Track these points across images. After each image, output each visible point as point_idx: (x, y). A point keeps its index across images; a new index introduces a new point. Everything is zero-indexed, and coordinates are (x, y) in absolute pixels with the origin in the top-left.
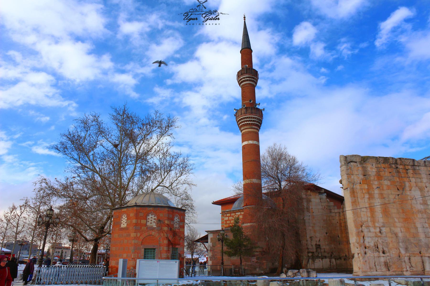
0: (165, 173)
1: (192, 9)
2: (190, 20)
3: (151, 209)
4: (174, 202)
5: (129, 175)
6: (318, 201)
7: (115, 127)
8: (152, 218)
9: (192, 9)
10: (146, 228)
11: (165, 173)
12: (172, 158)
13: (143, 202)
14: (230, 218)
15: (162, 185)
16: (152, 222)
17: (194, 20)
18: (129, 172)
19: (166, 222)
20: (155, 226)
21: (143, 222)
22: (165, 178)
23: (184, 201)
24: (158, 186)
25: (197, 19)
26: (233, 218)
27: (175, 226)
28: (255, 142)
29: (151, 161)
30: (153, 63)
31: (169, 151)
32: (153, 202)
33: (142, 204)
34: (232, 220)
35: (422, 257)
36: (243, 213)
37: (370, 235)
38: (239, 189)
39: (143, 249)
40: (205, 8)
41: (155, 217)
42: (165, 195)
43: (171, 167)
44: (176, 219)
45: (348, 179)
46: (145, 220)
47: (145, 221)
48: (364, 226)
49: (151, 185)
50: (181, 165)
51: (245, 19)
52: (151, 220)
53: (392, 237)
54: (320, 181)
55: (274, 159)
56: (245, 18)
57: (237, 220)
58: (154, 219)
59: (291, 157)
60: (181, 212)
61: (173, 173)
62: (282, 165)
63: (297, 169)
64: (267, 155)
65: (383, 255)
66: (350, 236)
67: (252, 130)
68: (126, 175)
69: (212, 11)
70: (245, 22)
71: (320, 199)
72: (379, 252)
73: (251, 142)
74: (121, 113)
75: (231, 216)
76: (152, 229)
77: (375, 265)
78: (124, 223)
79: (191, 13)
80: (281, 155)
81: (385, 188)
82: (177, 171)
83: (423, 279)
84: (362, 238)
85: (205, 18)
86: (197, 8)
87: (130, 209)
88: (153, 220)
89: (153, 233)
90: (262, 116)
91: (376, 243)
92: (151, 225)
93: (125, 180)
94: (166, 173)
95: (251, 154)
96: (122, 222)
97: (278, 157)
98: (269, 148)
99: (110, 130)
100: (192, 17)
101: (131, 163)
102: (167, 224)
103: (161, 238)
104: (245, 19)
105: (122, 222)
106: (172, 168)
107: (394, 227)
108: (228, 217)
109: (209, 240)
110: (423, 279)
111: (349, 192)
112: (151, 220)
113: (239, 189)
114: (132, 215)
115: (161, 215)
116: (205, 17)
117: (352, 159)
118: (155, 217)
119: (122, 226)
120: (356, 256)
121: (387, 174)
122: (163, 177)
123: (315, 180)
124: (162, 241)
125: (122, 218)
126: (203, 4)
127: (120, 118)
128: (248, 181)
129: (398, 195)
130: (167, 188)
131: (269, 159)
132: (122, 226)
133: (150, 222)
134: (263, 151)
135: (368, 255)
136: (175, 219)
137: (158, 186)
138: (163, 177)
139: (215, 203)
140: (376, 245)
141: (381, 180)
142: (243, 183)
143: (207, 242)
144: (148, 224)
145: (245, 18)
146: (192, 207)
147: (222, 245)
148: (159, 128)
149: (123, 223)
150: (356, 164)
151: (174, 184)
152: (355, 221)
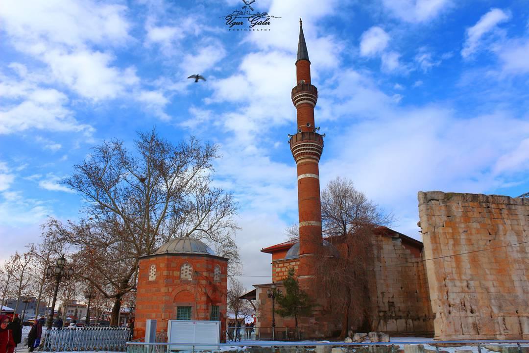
0: (202, 213)
1: (236, 11)
3: (186, 257)
4: (214, 249)
5: (158, 217)
6: (391, 248)
7: (141, 157)
8: (186, 269)
9: (236, 11)
10: (179, 281)
11: (202, 213)
12: (211, 195)
13: (176, 249)
14: (284, 269)
15: (199, 228)
16: (187, 274)
17: (239, 24)
18: (158, 212)
19: (205, 274)
20: (191, 279)
21: (176, 273)
22: (203, 219)
23: (227, 248)
24: (195, 229)
25: (242, 23)
26: (287, 270)
27: (215, 279)
28: (314, 176)
29: (185, 199)
30: (189, 78)
31: (208, 186)
32: (188, 249)
33: (175, 252)
34: (286, 271)
35: (519, 317)
36: (299, 263)
37: (455, 289)
38: (294, 234)
39: (176, 308)
40: (253, 10)
41: (191, 269)
42: (204, 241)
43: (210, 207)
44: (217, 270)
45: (428, 221)
46: (178, 271)
47: (179, 273)
48: (447, 278)
49: (186, 228)
50: (223, 204)
51: (301, 24)
52: (186, 272)
53: (482, 293)
54: (393, 223)
55: (337, 196)
56: (301, 22)
57: (291, 272)
58: (190, 270)
59: (358, 194)
60: (223, 262)
61: (212, 214)
62: (347, 204)
63: (366, 209)
64: (328, 191)
65: (472, 315)
66: (431, 291)
67: (310, 160)
68: (155, 216)
69: (261, 14)
70: (301, 27)
71: (394, 246)
72: (466, 311)
73: (308, 175)
74: (149, 140)
75: (284, 267)
76: (187, 282)
77: (461, 328)
78: (153, 275)
79: (235, 16)
80: (346, 191)
81: (474, 231)
82: (218, 211)
83: (520, 344)
84: (445, 293)
85: (253, 22)
86: (242, 10)
87: (160, 258)
88: (189, 272)
89: (189, 288)
90: (322, 143)
91: (462, 300)
92: (186, 277)
93: (154, 222)
94: (204, 214)
95: (309, 190)
96: (150, 274)
97: (342, 194)
98: (331, 182)
99: (135, 160)
100: (236, 21)
101: (161, 201)
102: (206, 277)
103: (198, 294)
104: (301, 24)
105: (150, 274)
106: (212, 207)
107: (485, 280)
108: (281, 267)
109: (257, 296)
110: (520, 344)
111: (429, 236)
112: (186, 272)
113: (294, 234)
114: (162, 265)
115: (198, 265)
116: (252, 21)
117: (433, 196)
118: (191, 269)
119: (150, 279)
120: (438, 315)
121: (476, 215)
122: (201, 219)
123: (388, 222)
124: (199, 297)
125: (150, 269)
126: (250, 5)
127: (148, 146)
128: (304, 224)
129: (490, 241)
130: (206, 232)
131: (331, 197)
132: (150, 279)
133: (185, 274)
134: (324, 187)
135: (453, 314)
136: (215, 270)
137: (195, 229)
138: (201, 219)
139: (253, 285)
140: (463, 302)
141: (469, 222)
142: (299, 225)
143: (255, 299)
144: (183, 276)
145: (301, 22)
146: (236, 255)
147: (274, 302)
148: (195, 158)
149: (152, 275)
150: (438, 202)
151: (215, 228)
152: (437, 273)
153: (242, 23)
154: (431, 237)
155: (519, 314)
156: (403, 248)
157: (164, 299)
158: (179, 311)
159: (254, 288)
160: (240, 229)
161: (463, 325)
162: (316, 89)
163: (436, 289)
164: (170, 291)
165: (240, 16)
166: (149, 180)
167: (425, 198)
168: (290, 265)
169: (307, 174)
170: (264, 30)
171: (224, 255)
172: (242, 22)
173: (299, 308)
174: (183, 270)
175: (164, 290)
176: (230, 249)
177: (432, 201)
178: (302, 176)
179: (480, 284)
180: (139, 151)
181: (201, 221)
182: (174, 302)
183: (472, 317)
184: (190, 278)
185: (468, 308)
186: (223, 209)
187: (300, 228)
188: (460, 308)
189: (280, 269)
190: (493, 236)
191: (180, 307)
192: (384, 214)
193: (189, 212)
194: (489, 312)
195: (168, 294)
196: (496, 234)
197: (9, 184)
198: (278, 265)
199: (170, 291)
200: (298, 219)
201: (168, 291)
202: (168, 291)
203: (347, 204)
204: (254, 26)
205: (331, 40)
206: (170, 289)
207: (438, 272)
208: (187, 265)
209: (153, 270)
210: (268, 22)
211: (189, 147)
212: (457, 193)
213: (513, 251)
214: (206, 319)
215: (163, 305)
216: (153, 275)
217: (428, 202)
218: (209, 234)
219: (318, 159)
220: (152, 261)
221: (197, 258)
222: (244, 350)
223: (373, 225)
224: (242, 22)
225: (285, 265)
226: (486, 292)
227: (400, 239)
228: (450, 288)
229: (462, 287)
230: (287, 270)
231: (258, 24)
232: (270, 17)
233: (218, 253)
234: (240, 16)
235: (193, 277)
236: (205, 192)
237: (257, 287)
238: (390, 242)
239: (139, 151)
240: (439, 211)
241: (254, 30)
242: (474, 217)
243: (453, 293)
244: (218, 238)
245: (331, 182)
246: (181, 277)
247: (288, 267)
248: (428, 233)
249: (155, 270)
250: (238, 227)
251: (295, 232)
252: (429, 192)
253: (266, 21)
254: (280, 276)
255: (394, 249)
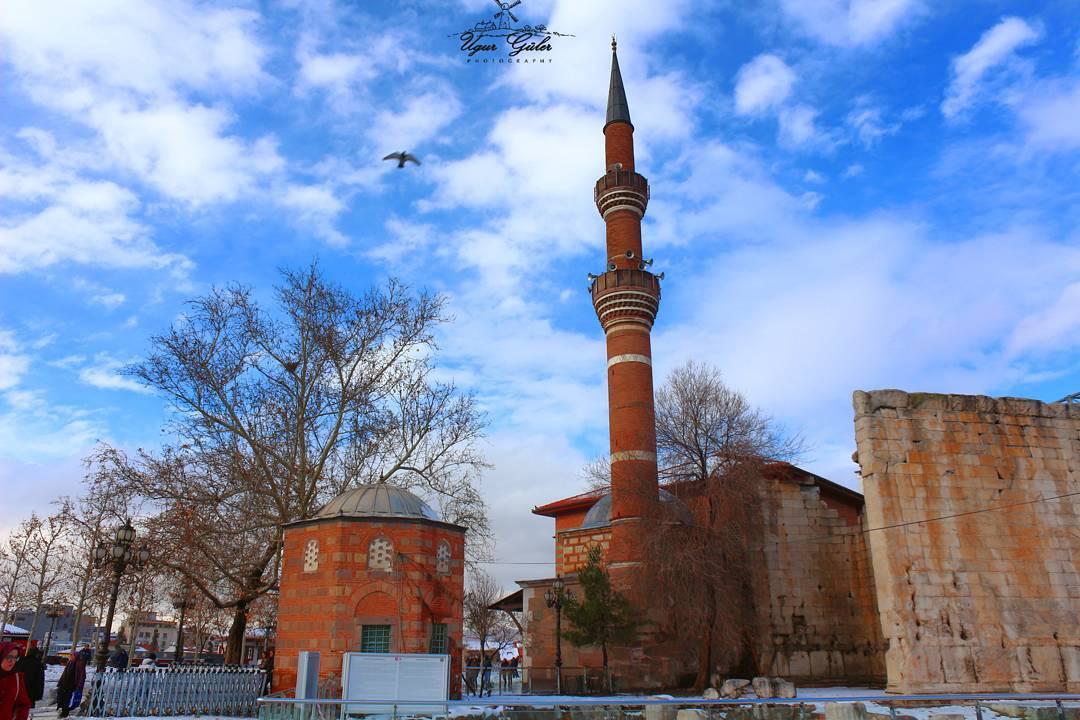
0: (413, 435)
1: (483, 23)
2: (477, 49)
3: (380, 525)
4: (437, 507)
5: (323, 442)
6: (798, 505)
7: (289, 319)
8: (381, 548)
9: (483, 23)
10: (365, 573)
11: (413, 435)
12: (431, 398)
13: (359, 509)
14: (579, 549)
15: (407, 465)
16: (382, 558)
17: (487, 49)
18: (323, 432)
19: (418, 559)
20: (391, 570)
21: (360, 558)
22: (414, 448)
23: (462, 506)
24: (398, 467)
25: (494, 48)
26: (586, 550)
27: (439, 568)
28: (640, 358)
29: (379, 405)
31: (424, 380)
32: (384, 507)
33: (357, 515)
34: (583, 553)
36: (609, 536)
37: (929, 590)
38: (601, 477)
39: (360, 628)
40: (516, 21)
41: (390, 548)
42: (416, 491)
43: (429, 421)
44: (443, 552)
45: (874, 450)
46: (364, 552)
47: (365, 556)
48: (913, 568)
49: (379, 465)
50: (456, 416)
51: (615, 49)
52: (380, 555)
53: (985, 597)
54: (803, 456)
55: (687, 401)
56: (614, 44)
57: (595, 555)
58: (388, 551)
59: (731, 396)
60: (455, 534)
61: (434, 436)
62: (708, 417)
63: (747, 426)
64: (670, 389)
65: (963, 642)
66: (880, 594)
67: (633, 327)
68: (316, 441)
69: (533, 28)
70: (615, 55)
71: (804, 501)
72: (952, 635)
73: (629, 358)
74: (305, 285)
75: (579, 544)
76: (382, 576)
77: (942, 668)
78: (312, 561)
79: (479, 33)
80: (707, 390)
81: (967, 472)
82: (444, 431)
83: (1063, 702)
84: (909, 598)
85: (516, 46)
86: (493, 20)
87: (327, 526)
88: (385, 555)
89: (385, 587)
90: (657, 291)
91: (944, 613)
92: (381, 566)
93: (313, 454)
94: (417, 437)
95: (631, 388)
96: (307, 558)
97: (699, 396)
98: (676, 372)
99: (275, 327)
100: (482, 42)
101: (328, 409)
102: (421, 564)
103: (404, 600)
104: (615, 49)
105: (307, 558)
106: (433, 423)
107: (989, 571)
108: (574, 545)
109: (526, 605)
110: (1063, 702)
111: (876, 482)
112: (380, 555)
113: (601, 477)
114: (331, 541)
115: (405, 541)
116: (515, 42)
117: (884, 399)
118: (390, 548)
119: (307, 569)
120: (894, 643)
121: (972, 438)
122: (410, 446)
123: (792, 453)
124: (406, 606)
125: (307, 548)
126: (511, 10)
127: (302, 297)
128: (621, 456)
129: (1000, 491)
130: (420, 473)
131: (676, 401)
132: (307, 569)
133: (377, 558)
134: (661, 381)
135: (924, 641)
136: (440, 552)
137: (398, 467)
138: (410, 446)
139: (517, 582)
140: (945, 617)
141: (957, 453)
142: (610, 460)
143: (521, 610)
144: (373, 563)
145: (614, 44)
146: (482, 521)
147: (559, 616)
148: (398, 321)
149: (310, 561)
150: (894, 412)
151: (438, 464)
152: (892, 557)
153: (494, 48)
154: (880, 484)
156: (823, 507)
157: (334, 610)
158: (364, 634)
159: (518, 588)
160: (489, 466)
161: (944, 663)
162: (646, 181)
163: (890, 590)
164: (348, 593)
165: (490, 33)
166: (305, 367)
167: (867, 404)
168: (592, 540)
169: (628, 356)
170: (538, 60)
171: (457, 520)
172: (494, 46)
173: (611, 627)
174: (373, 551)
175: (334, 591)
176: (469, 507)
177: (883, 411)
178: (617, 360)
179: (980, 578)
180: (285, 308)
181: (411, 451)
182: (355, 616)
183: (963, 646)
184: (388, 568)
185: (956, 629)
186: (456, 426)
187: (612, 465)
188: (940, 628)
189: (571, 548)
190: (1008, 481)
191: (368, 626)
192: (784, 437)
193: (385, 433)
194: (999, 637)
195: (342, 599)
196: (1013, 477)
198: (568, 542)
199: (348, 593)
200: (608, 446)
201: (344, 593)
202: (344, 593)
203: (708, 417)
204: (518, 52)
205: (676, 81)
206: (348, 590)
207: (894, 554)
208: (381, 541)
209: (311, 551)
211: (386, 301)
212: (934, 394)
213: (1046, 513)
214: (421, 650)
215: (334, 623)
216: (312, 561)
217: (874, 412)
218: (426, 478)
219: (649, 324)
220: (310, 532)
221: (402, 526)
222: (498, 714)
223: (761, 460)
224: (494, 46)
225: (582, 541)
226: (992, 595)
227: (818, 488)
228: (918, 588)
229: (943, 586)
230: (586, 550)
231: (527, 49)
233: (446, 516)
234: (490, 33)
235: (395, 564)
236: (418, 392)
237: (526, 586)
238: (796, 494)
239: (285, 308)
240: (896, 430)
241: (518, 61)
242: (968, 444)
243: (925, 597)
244: (446, 486)
245: (676, 372)
246: (370, 565)
247: (588, 544)
248: (874, 475)
249: (317, 550)
250: (486, 462)
251: (603, 473)
252: (875, 392)
254: (572, 563)
255: (805, 508)
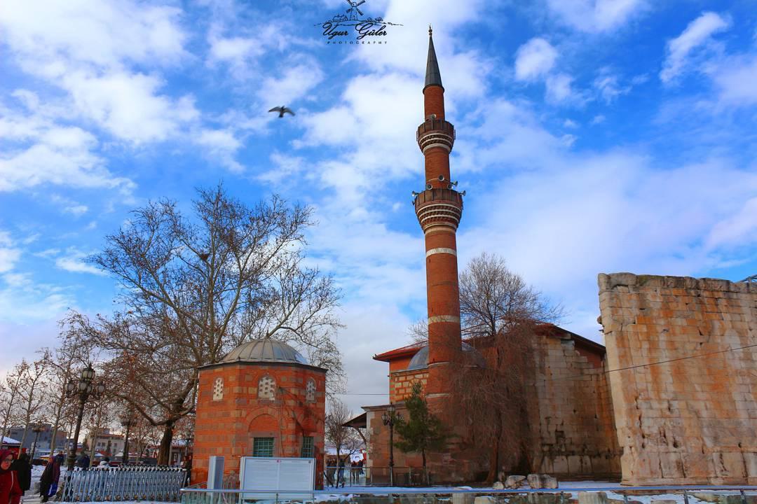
0: (290, 304)
1: (338, 16)
3: (266, 368)
4: (307, 355)
5: (227, 309)
6: (559, 354)
7: (202, 224)
8: (267, 384)
9: (338, 16)
10: (256, 401)
11: (290, 304)
12: (302, 279)
13: (252, 356)
14: (406, 384)
15: (285, 326)
16: (268, 391)
17: (341, 35)
18: (227, 303)
19: (293, 391)
20: (274, 399)
21: (252, 390)
22: (290, 313)
23: (324, 354)
24: (279, 327)
25: (346, 33)
26: (410, 385)
27: (308, 398)
28: (449, 251)
29: (265, 284)
31: (297, 266)
32: (269, 355)
33: (250, 360)
34: (409, 387)
35: (742, 452)
36: (427, 376)
37: (651, 413)
38: (421, 334)
39: (252, 440)
40: (361, 14)
41: (274, 383)
42: (292, 344)
43: (301, 295)
44: (311, 386)
45: (613, 315)
46: (255, 387)
47: (256, 389)
48: (640, 397)
49: (266, 325)
50: (319, 291)
51: (431, 34)
52: (266, 388)
53: (690, 418)
54: (563, 319)
55: (482, 281)
56: (431, 31)
57: (417, 388)
58: (272, 386)
59: (513, 277)
60: (319, 374)
61: (304, 305)
62: (496, 292)
63: (524, 298)
64: (469, 272)
65: (675, 449)
66: (617, 416)
67: (444, 229)
68: (222, 309)
69: (374, 19)
70: (431, 38)
71: (564, 351)
72: (667, 444)
73: (441, 250)
74: (213, 200)
75: (406, 381)
76: (268, 403)
77: (660, 468)
78: (219, 393)
79: (336, 23)
80: (495, 273)
81: (678, 330)
82: (311, 302)
83: (745, 491)
84: (637, 419)
85: (362, 32)
86: (346, 14)
87: (229, 368)
88: (270, 388)
89: (270, 411)
90: (460, 204)
91: (661, 429)
92: (267, 396)
93: (220, 318)
94: (292, 306)
95: (442, 272)
96: (215, 391)
97: (490, 277)
98: (474, 260)
99: (193, 229)
100: (338, 29)
101: (230, 286)
102: (295, 395)
103: (283, 420)
104: (431, 34)
105: (215, 391)
106: (303, 296)
107: (694, 400)
108: (402, 382)
109: (368, 423)
110: (745, 491)
111: (614, 338)
112: (266, 388)
113: (421, 334)
114: (232, 379)
115: (284, 379)
116: (361, 30)
117: (620, 280)
118: (274, 383)
119: (215, 398)
120: (627, 450)
121: (681, 307)
122: (287, 312)
123: (555, 317)
124: (284, 424)
125: (215, 384)
126: (358, 7)
127: (212, 208)
128: (435, 319)
129: (701, 344)
130: (295, 331)
131: (474, 281)
132: (215, 398)
133: (264, 391)
134: (463, 267)
135: (648, 449)
136: (308, 386)
137: (279, 327)
138: (287, 312)
139: (362, 408)
140: (662, 432)
141: (671, 317)
142: (427, 322)
143: (365, 427)
144: (261, 394)
145: (431, 31)
146: (338, 365)
147: (392, 431)
148: (279, 225)
149: (217, 393)
150: (626, 288)
151: (307, 325)
152: (625, 390)
153: (346, 33)
154: (617, 339)
155: (742, 449)
156: (577, 355)
157: (234, 427)
158: (255, 444)
159: (363, 412)
160: (343, 326)
161: (662, 464)
162: (453, 126)
163: (624, 413)
164: (244, 415)
165: (344, 23)
166: (214, 257)
167: (607, 283)
168: (415, 378)
169: (440, 249)
170: (377, 42)
171: (321, 364)
172: (346, 32)
173: (428, 439)
174: (262, 386)
175: (234, 414)
176: (329, 355)
177: (619, 287)
178: (432, 252)
179: (687, 405)
180: (200, 216)
181: (288, 316)
182: (249, 431)
183: (675, 452)
184: (272, 397)
185: (670, 440)
186: (320, 298)
187: (429, 326)
188: (659, 440)
189: (400, 384)
190: (706, 337)
191: (258, 438)
192: (550, 306)
193: (270, 303)
194: (700, 446)
195: (240, 419)
196: (710, 334)
197: (13, 262)
198: (398, 379)
199: (244, 415)
200: (426, 313)
201: (241, 415)
202: (241, 415)
203: (496, 292)
204: (363, 36)
205: (474, 57)
206: (244, 413)
207: (626, 388)
208: (267, 379)
209: (218, 385)
210: (383, 31)
211: (270, 210)
212: (654, 276)
213: (734, 359)
214: (295, 455)
215: (234, 436)
216: (219, 393)
217: (612, 289)
218: (299, 335)
219: (455, 227)
220: (217, 373)
221: (282, 368)
223: (534, 322)
224: (346, 32)
225: (408, 379)
226: (696, 417)
227: (573, 342)
228: (644, 411)
229: (661, 410)
230: (410, 385)
231: (369, 34)
232: (387, 25)
233: (312, 361)
234: (344, 23)
235: (277, 395)
236: (293, 274)
237: (368, 410)
238: (558, 346)
239: (200, 216)
240: (628, 301)
241: (363, 43)
242: (679, 310)
243: (648, 418)
244: (312, 340)
245: (474, 260)
246: (259, 396)
247: (412, 381)
248: (613, 333)
249: (222, 385)
250: (340, 324)
251: (423, 331)
252: (613, 275)
253: (381, 29)
254: (401, 394)
255: (564, 355)
